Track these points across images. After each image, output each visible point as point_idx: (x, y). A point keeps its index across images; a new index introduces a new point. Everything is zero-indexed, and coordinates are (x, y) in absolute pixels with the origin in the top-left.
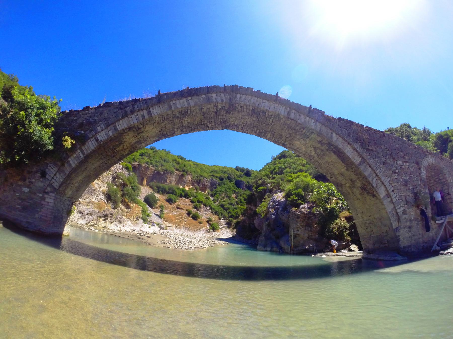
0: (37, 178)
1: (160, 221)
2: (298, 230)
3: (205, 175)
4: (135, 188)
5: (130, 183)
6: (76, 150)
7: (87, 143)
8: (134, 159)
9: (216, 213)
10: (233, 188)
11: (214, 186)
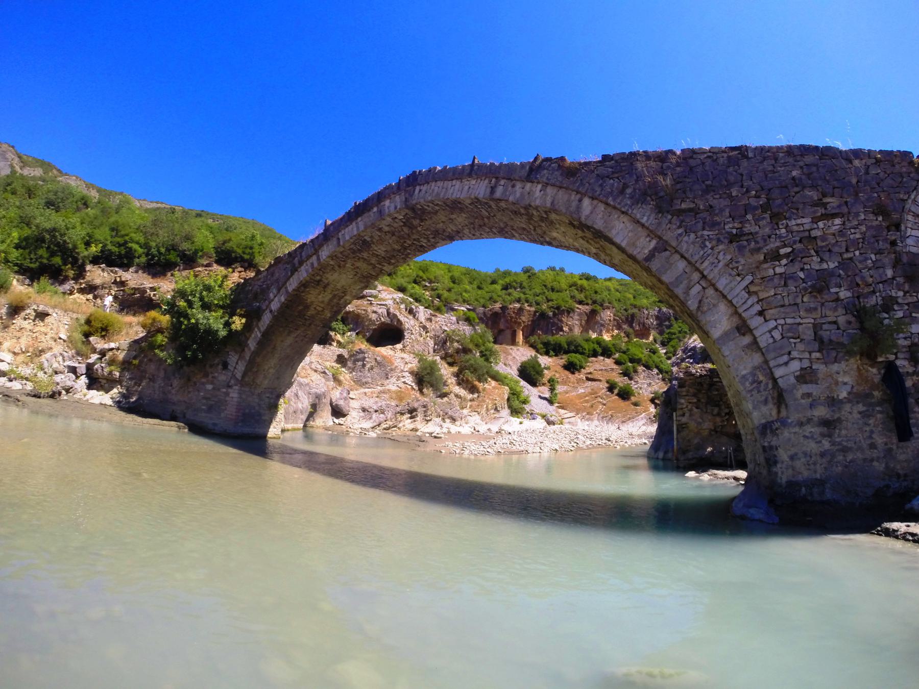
1: (550, 410)
4: (488, 353)
5: (477, 346)
8: (491, 298)
11: (667, 323)
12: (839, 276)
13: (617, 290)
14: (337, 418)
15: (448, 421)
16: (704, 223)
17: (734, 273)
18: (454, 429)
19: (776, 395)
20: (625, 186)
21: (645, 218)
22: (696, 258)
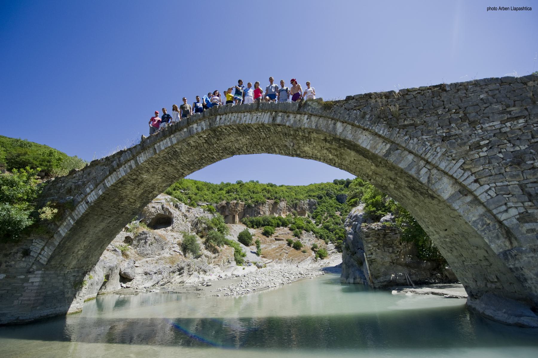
0: (18, 259)
2: (372, 254)
3: (301, 197)
4: (222, 229)
5: (216, 225)
6: (66, 218)
7: (77, 208)
8: (220, 198)
9: (321, 237)
10: (335, 205)
12: (531, 153)
13: (286, 191)
14: (124, 283)
15: (201, 273)
16: (422, 132)
17: (450, 158)
18: (206, 278)
19: (504, 232)
20: (365, 114)
21: (381, 132)
22: (421, 152)
